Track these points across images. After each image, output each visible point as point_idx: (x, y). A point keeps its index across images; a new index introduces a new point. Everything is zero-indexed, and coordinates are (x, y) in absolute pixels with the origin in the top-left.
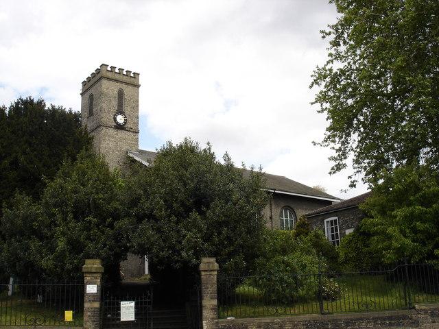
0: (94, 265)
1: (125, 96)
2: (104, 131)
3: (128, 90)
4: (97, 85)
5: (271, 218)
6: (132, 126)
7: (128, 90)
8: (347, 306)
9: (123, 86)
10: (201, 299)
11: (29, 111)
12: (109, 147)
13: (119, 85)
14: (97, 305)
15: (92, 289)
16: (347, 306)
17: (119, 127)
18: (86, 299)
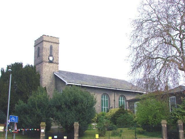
0: (43, 124)
1: (53, 48)
2: (44, 64)
3: (54, 46)
4: (41, 44)
5: (114, 100)
6: (56, 61)
7: (54, 46)
8: (128, 135)
9: (52, 44)
10: (74, 134)
11: (16, 67)
12: (46, 80)
13: (51, 44)
14: (44, 135)
15: (43, 131)
16: (128, 135)
17: (51, 62)
18: (41, 133)
